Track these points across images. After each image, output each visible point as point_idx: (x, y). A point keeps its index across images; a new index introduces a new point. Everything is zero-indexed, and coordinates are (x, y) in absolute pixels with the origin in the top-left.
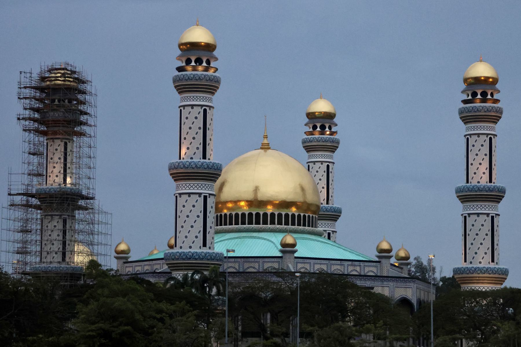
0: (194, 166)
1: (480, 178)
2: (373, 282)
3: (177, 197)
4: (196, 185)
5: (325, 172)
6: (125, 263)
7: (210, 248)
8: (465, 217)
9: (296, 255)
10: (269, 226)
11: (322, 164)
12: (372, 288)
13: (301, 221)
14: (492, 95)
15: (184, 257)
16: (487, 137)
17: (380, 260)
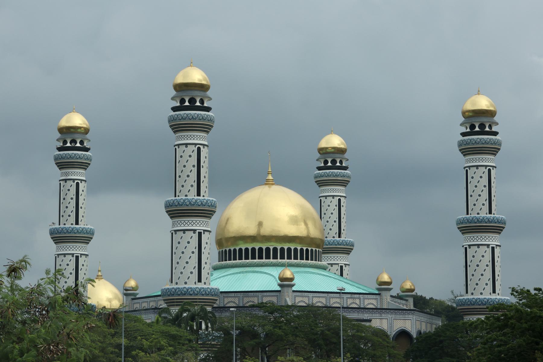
0: (188, 203)
1: (69, 224)
2: (370, 315)
3: (172, 233)
4: (190, 222)
5: (336, 206)
6: (133, 299)
7: (205, 283)
8: (466, 248)
9: (294, 288)
10: (272, 260)
11: (333, 198)
12: (370, 321)
13: (305, 255)
14: (490, 127)
15: (179, 293)
16: (486, 168)
17: (380, 292)
